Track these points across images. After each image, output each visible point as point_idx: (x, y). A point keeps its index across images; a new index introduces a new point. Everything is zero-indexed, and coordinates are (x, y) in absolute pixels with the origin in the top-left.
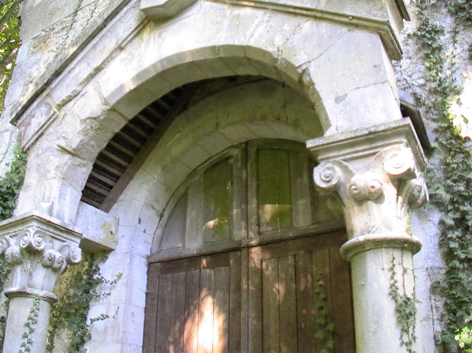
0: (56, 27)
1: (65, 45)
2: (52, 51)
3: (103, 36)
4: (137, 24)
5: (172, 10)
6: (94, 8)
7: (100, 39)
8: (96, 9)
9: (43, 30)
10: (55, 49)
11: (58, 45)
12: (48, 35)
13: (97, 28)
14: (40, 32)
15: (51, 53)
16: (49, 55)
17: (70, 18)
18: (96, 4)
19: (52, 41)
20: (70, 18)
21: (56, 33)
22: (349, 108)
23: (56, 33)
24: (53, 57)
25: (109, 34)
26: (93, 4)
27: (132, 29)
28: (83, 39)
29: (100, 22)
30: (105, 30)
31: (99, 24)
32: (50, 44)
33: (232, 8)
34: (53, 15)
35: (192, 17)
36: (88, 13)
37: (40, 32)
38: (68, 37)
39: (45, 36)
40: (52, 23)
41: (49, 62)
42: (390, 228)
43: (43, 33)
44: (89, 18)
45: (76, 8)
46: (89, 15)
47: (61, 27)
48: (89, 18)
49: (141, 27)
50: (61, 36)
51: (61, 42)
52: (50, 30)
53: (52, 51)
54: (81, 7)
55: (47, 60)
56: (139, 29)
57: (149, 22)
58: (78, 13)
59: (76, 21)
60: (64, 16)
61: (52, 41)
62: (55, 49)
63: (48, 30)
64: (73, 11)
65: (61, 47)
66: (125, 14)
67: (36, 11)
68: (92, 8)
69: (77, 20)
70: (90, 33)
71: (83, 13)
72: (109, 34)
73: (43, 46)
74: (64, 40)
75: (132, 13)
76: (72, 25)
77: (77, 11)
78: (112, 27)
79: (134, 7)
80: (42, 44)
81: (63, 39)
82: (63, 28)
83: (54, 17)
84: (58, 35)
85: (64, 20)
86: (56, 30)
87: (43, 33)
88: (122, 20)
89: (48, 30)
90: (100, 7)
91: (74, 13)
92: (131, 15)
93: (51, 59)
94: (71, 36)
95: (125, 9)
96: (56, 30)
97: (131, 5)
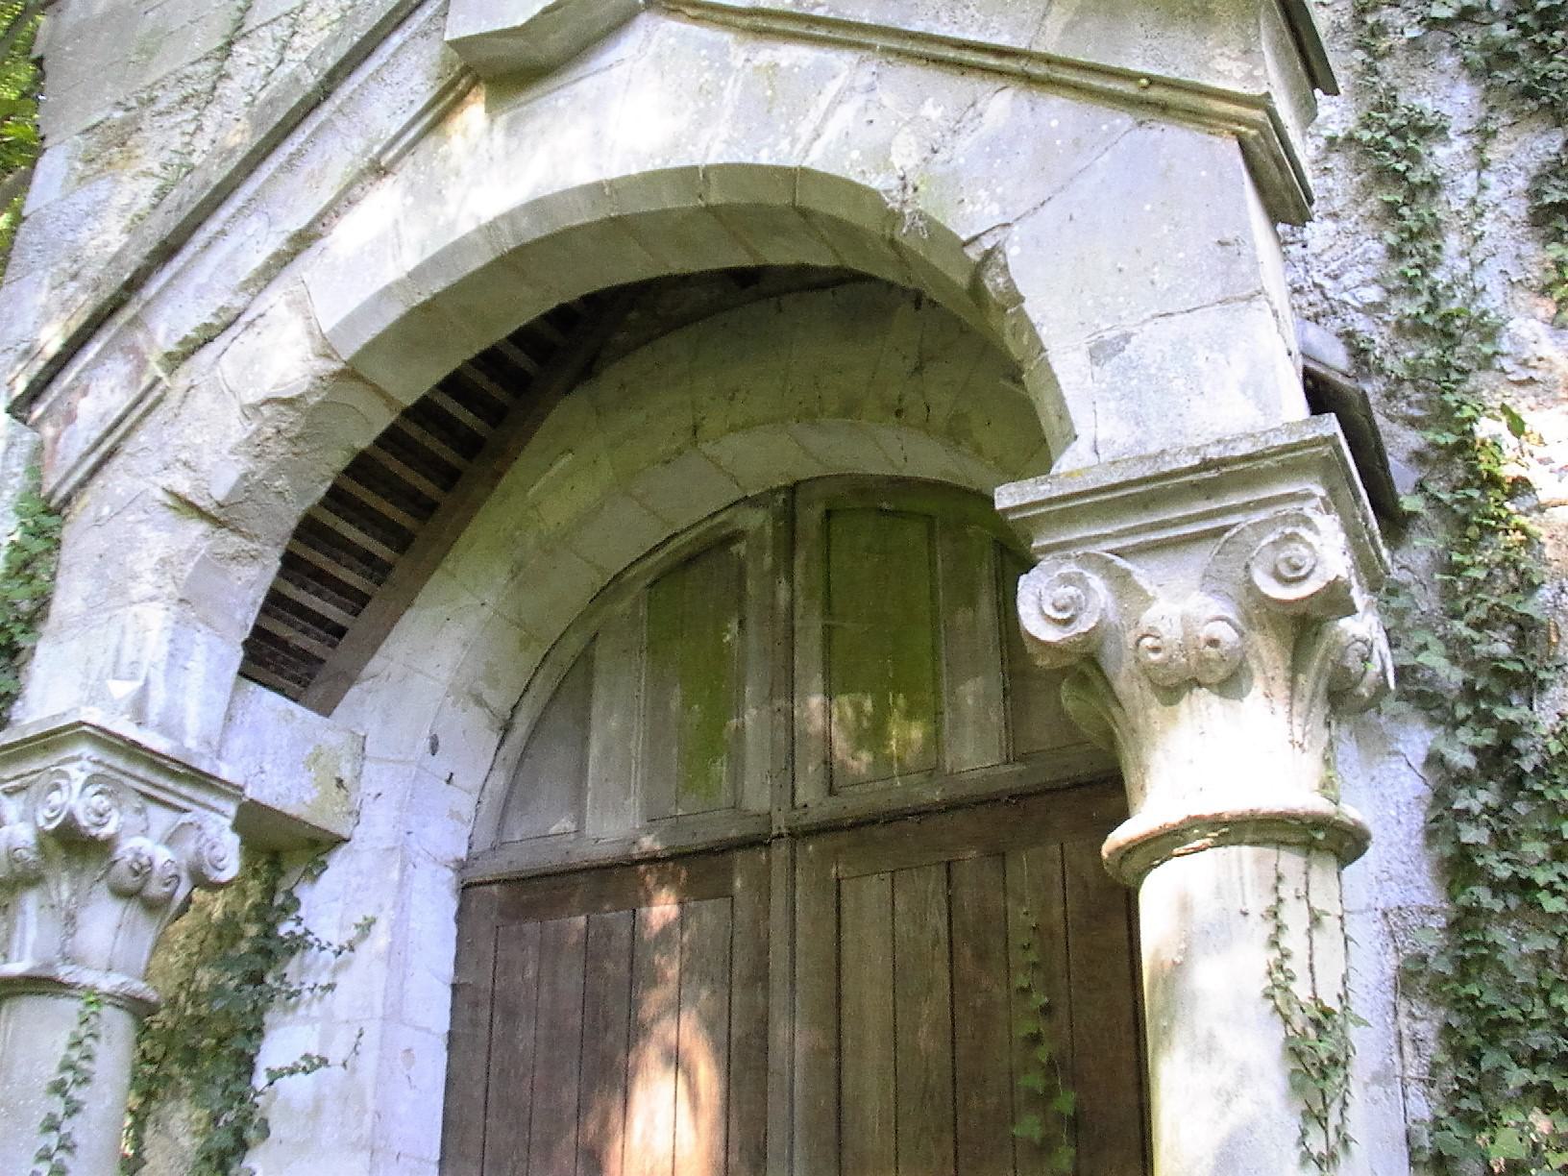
1: (190, 154)
2: (148, 174)
5: (554, 44)
6: (288, 32)
7: (311, 140)
10: (157, 169)
11: (165, 155)
12: (134, 119)
13: (301, 102)
14: (107, 111)
16: (135, 187)
21: (160, 114)
23: (160, 114)
24: (149, 193)
25: (341, 124)
26: (286, 21)
27: (419, 106)
29: (311, 80)
31: (309, 89)
32: (139, 152)
33: (750, 42)
34: (151, 54)
35: (615, 71)
36: (268, 51)
37: (107, 111)
38: (200, 128)
39: (124, 123)
41: (135, 209)
44: (272, 65)
46: (271, 56)
47: (176, 96)
51: (177, 142)
52: (142, 103)
53: (148, 174)
54: (244, 30)
57: (475, 82)
58: (236, 48)
59: (228, 76)
62: (157, 169)
63: (133, 103)
64: (220, 42)
66: (394, 55)
69: (232, 71)
70: (278, 118)
71: (251, 48)
72: (341, 124)
74: (187, 139)
76: (214, 88)
77: (230, 43)
79: (425, 34)
82: (185, 100)
83: (155, 60)
84: (167, 122)
86: (161, 106)
87: (119, 114)
88: (386, 76)
89: (133, 103)
90: (307, 31)
91: (220, 49)
93: (144, 202)
95: (396, 39)
96: (161, 106)
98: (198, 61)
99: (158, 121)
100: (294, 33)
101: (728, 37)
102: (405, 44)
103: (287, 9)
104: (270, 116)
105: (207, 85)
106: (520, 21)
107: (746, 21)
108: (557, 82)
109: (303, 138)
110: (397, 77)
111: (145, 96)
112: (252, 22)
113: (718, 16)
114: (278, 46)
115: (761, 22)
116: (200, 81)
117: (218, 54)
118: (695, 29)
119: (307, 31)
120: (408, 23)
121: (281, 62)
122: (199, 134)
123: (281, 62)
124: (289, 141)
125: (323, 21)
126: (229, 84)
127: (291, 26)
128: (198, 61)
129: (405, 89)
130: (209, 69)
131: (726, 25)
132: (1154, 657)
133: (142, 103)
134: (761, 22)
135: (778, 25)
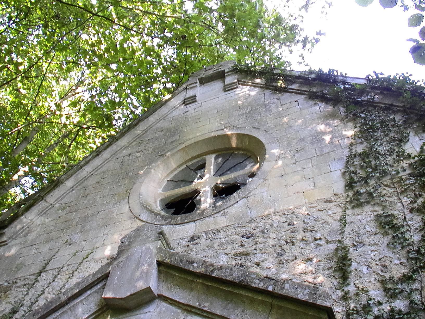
0: (19, 281)
1: (23, 300)
2: (10, 303)
3: (63, 312)
4: (97, 309)
5: (131, 304)
6: (57, 273)
7: (60, 315)
8: (59, 276)
9: (7, 281)
10: (13, 303)
11: (16, 299)
12: (10, 286)
13: (59, 304)
14: (3, 282)
15: (8, 304)
16: (6, 306)
17: (34, 277)
18: (60, 271)
19: (12, 293)
20: (34, 277)
21: (18, 287)
22: (12, 36)
23: (18, 287)
24: (9, 308)
25: (69, 312)
26: (57, 270)
27: (91, 313)
28: (44, 311)
29: (64, 299)
30: (66, 308)
31: (62, 301)
32: (9, 296)
33: (185, 314)
34: (19, 270)
35: (148, 314)
36: (51, 277)
37: (3, 282)
38: (27, 294)
39: (7, 287)
40: (16, 277)
41: (4, 312)
42: (167, 309)
43: (6, 284)
44: (51, 282)
45: (41, 269)
46: (51, 279)
47: (23, 283)
48: (51, 282)
49: (100, 312)
50: (21, 291)
51: (20, 296)
52: (13, 283)
53: (10, 303)
54: (45, 270)
55: (3, 311)
56: (97, 314)
57: (108, 309)
58: (42, 274)
59: (38, 281)
60: (28, 274)
61: (12, 293)
62: (13, 303)
63: (11, 282)
64: (38, 271)
65: (19, 301)
66: (87, 297)
67: (5, 261)
68: (56, 273)
69: (40, 280)
70: (52, 308)
71: (46, 275)
72: (69, 312)
73: (3, 296)
74: (23, 296)
75: (94, 297)
76: (34, 284)
77: (41, 272)
78: (73, 306)
79: (97, 293)
80: (3, 294)
81: (23, 294)
82: (25, 285)
83: (20, 271)
84: (19, 290)
85: (28, 277)
86: (18, 285)
87: (6, 284)
88: (84, 302)
89: (11, 282)
90: (62, 274)
91: (38, 273)
92: (92, 299)
93: (7, 311)
94: (30, 294)
95: (89, 292)
96: (18, 285)
97: (94, 290)
98: (31, 275)
99: (16, 289)
100: (59, 274)
101: (179, 311)
102: (91, 294)
103: (58, 267)
104: (50, 306)
105: (32, 283)
106: (124, 297)
107: (185, 307)
108: (131, 314)
109: (58, 314)
110: (87, 303)
111: (14, 281)
112: (48, 268)
113: (178, 304)
114: (54, 276)
115: (189, 309)
116: (30, 281)
117: (37, 275)
118: (171, 307)
119: (62, 274)
120: (93, 289)
121: (54, 281)
122: (27, 296)
123: (54, 281)
124: (54, 314)
125: (67, 272)
126: (38, 284)
127: (58, 272)
128: (31, 275)
129: (88, 307)
130: (34, 278)
131: (180, 307)
132: (256, 270)
133: (13, 283)
134: (189, 309)
135: (194, 310)
